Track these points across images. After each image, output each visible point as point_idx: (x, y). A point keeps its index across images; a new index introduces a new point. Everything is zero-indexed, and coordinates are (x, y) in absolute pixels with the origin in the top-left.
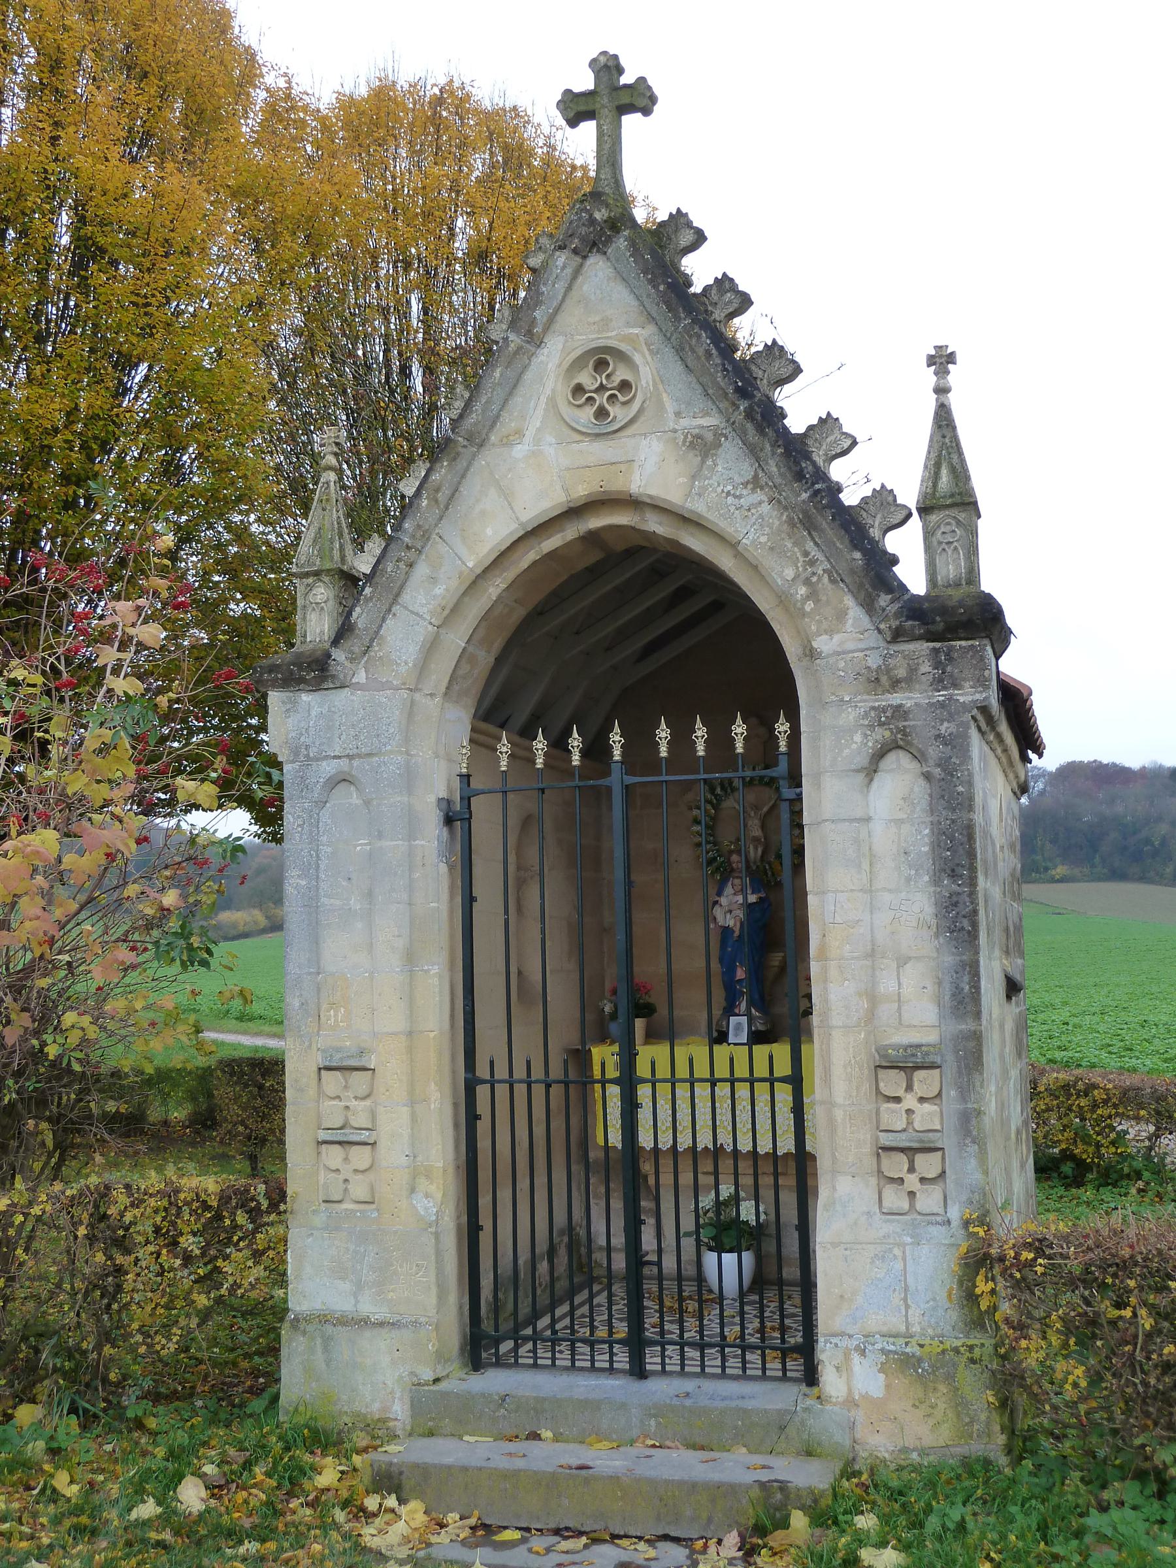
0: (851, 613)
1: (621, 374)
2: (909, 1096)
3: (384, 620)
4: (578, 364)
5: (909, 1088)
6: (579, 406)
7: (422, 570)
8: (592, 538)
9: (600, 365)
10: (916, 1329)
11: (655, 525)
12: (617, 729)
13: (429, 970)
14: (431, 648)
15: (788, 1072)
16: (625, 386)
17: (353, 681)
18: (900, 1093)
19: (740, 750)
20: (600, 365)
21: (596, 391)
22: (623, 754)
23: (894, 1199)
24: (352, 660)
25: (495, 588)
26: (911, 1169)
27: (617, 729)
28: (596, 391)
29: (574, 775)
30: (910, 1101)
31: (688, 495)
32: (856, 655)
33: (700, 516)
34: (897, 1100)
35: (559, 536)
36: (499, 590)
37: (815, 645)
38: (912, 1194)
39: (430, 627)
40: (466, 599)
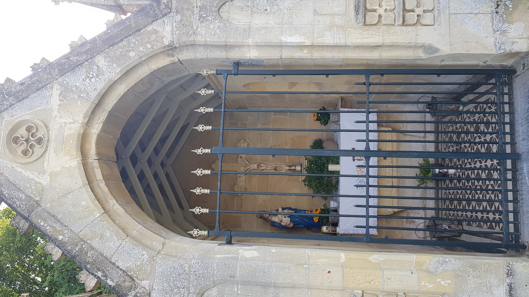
0: (155, 28)
1: (22, 132)
2: (379, 11)
3: (118, 267)
4: (12, 151)
5: (375, 11)
6: (33, 153)
7: (96, 243)
8: (101, 158)
9: (16, 140)
10: (489, 10)
11: (96, 129)
12: (195, 151)
13: (308, 255)
14: (138, 242)
15: (363, 77)
16: (29, 129)
17: (148, 289)
18: (377, 14)
19: (210, 128)
20: (16, 140)
21: (28, 143)
22: (207, 188)
23: (428, 19)
24: (136, 288)
25: (114, 204)
26: (413, 11)
27: (195, 151)
28: (28, 143)
29: (213, 212)
30: (381, 11)
31: (87, 100)
32: (174, 26)
33: (98, 95)
34: (380, 16)
35: (95, 170)
36: (117, 204)
37: (167, 44)
38: (425, 11)
39: (126, 240)
40: (117, 222)
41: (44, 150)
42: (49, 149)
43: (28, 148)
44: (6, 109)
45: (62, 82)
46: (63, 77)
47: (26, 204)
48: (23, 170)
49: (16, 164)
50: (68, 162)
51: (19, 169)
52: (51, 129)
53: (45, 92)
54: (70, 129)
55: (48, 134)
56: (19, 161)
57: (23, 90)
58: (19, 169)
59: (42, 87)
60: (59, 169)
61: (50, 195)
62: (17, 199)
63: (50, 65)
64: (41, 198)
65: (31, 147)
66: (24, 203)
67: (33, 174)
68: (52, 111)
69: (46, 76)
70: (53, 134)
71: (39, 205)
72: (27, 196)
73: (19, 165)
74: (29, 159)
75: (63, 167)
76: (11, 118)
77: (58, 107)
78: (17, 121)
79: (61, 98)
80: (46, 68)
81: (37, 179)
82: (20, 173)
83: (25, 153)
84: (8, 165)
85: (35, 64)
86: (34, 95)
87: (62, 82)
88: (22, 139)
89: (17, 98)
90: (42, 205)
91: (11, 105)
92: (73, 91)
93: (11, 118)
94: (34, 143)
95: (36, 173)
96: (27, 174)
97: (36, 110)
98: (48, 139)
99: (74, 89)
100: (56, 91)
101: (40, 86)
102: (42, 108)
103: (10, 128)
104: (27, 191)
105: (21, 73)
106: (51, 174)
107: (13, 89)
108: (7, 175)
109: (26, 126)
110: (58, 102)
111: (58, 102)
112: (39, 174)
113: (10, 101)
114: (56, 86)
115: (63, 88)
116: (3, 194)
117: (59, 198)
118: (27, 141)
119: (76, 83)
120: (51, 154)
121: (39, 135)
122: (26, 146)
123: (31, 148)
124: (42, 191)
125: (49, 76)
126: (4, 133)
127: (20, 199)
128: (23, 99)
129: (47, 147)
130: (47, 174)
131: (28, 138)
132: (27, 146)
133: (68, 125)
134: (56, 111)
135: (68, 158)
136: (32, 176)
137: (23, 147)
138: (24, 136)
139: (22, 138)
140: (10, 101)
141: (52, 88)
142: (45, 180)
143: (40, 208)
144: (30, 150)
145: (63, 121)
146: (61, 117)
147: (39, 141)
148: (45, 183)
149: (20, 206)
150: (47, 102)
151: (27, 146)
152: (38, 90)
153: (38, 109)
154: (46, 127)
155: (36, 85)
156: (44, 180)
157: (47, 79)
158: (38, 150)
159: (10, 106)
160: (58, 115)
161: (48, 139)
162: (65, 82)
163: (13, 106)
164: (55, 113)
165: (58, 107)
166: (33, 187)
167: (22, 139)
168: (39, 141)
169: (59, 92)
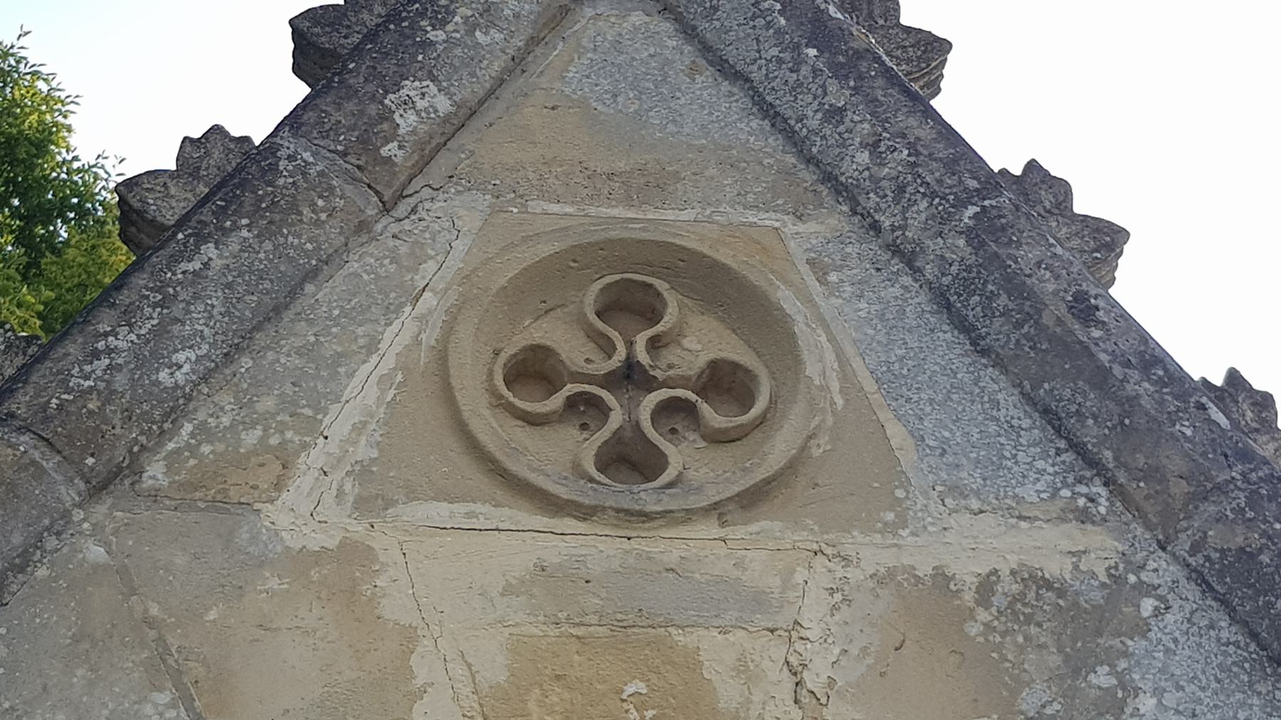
1: (701, 341)
4: (541, 284)
6: (533, 421)
9: (631, 305)
16: (725, 382)
20: (631, 305)
21: (609, 381)
28: (611, 381)
41: (562, 492)
42: (569, 524)
43: (570, 389)
44: (875, 227)
45: (1146, 589)
46: (1191, 591)
47: (109, 395)
48: (389, 362)
49: (439, 319)
50: (459, 671)
51: (398, 336)
52: (738, 532)
53: (1037, 470)
54: (745, 670)
55: (689, 516)
56: (465, 331)
57: (1033, 316)
58: (398, 336)
59: (1077, 447)
60: (395, 608)
61: (180, 560)
62: (160, 332)
63: (1090, 306)
64: (154, 496)
65: (584, 409)
66: (121, 381)
67: (359, 428)
68: (892, 529)
69: (1174, 463)
70: (700, 547)
71: (98, 487)
72: (176, 406)
73: (430, 337)
74: (484, 400)
75: (409, 638)
76: (800, 258)
77: (925, 570)
78: (786, 299)
79: (1009, 586)
80: (1246, 455)
81: (316, 457)
82: (372, 347)
83: (533, 369)
84: (431, 266)
85: (1062, 190)
86: (1009, 401)
87: (1146, 589)
88: (641, 341)
89: (968, 287)
90: (101, 510)
91: (908, 258)
92: (1077, 667)
93: (800, 258)
94: (616, 419)
95: (363, 451)
96: (363, 393)
97: (885, 416)
98: (646, 516)
99: (1102, 678)
100: (1069, 545)
101: (1090, 433)
102: (907, 457)
103: (724, 256)
104: (225, 399)
105: (992, 111)
106: (353, 554)
107: (1029, 255)
108: (354, 266)
109: (745, 357)
110: (967, 571)
111: (967, 571)
112: (363, 472)
113: (934, 245)
114: (1100, 548)
115: (1098, 596)
116: (201, 238)
117: (150, 622)
118: (631, 377)
119: (1158, 692)
120: (528, 542)
121: (679, 455)
122: (590, 369)
123: (572, 403)
124: (220, 504)
125: (1180, 488)
126: (681, 221)
127: (154, 350)
128: (963, 326)
129: (586, 513)
130: (358, 528)
131: (650, 384)
132: (589, 379)
133: (779, 652)
134: (888, 559)
135: (495, 670)
136: (339, 422)
137: (575, 351)
138: (670, 355)
139: (655, 344)
140: (934, 245)
141: (1084, 517)
142: (305, 512)
143: (69, 494)
144: (557, 401)
145: (813, 615)
146: (841, 596)
147: (631, 459)
148: (284, 520)
149: (96, 355)
150: (956, 490)
151: (589, 379)
152: (1049, 416)
153: (896, 433)
154: (752, 499)
155: (1092, 400)
156: (305, 508)
157: (1153, 474)
158: (562, 454)
159: (894, 249)
160: (854, 574)
161: (646, 516)
162: (1148, 605)
163: (896, 265)
164: (872, 554)
165: (925, 570)
166: (251, 438)
167: (641, 341)
168: (631, 459)
169: (1057, 567)
